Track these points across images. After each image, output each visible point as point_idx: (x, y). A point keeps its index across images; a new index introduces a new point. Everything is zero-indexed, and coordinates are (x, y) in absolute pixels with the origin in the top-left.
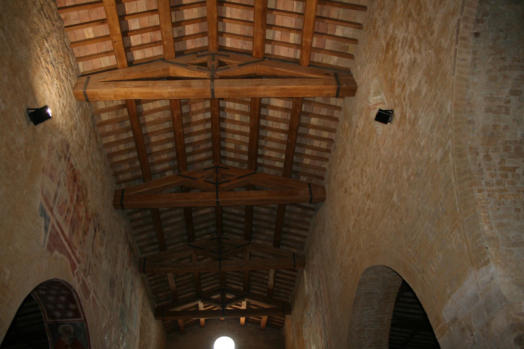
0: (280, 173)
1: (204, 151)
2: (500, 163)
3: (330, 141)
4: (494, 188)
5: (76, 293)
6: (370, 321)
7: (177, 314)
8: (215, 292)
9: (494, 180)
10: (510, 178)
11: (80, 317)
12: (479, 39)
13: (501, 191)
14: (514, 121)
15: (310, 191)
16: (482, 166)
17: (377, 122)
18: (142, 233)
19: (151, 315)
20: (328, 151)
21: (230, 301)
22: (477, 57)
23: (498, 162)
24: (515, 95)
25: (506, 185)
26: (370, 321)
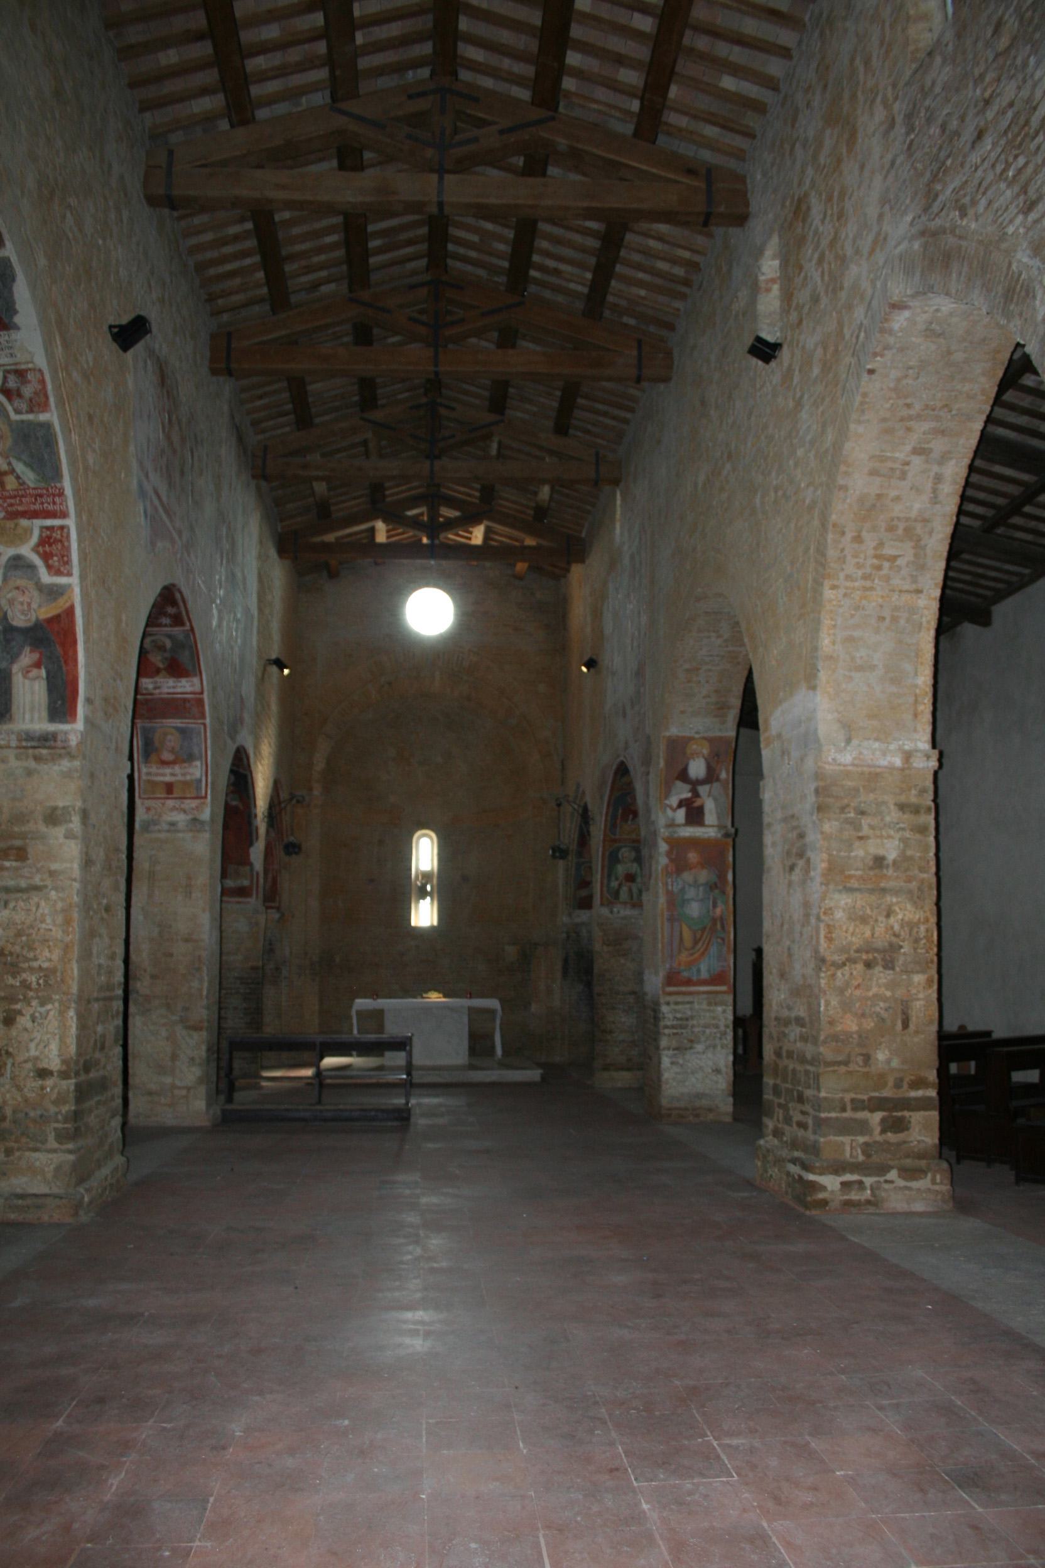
0: (579, 305)
1: (410, 243)
2: (875, 548)
3: (694, 266)
4: (857, 584)
5: (181, 593)
6: (711, 656)
7: (326, 547)
8: (415, 501)
9: (860, 573)
10: (885, 571)
11: (182, 624)
12: (873, 377)
13: (865, 589)
14: (911, 489)
15: (640, 358)
16: (846, 552)
17: (749, 357)
18: (260, 397)
19: (273, 553)
20: (687, 283)
21: (450, 524)
22: (867, 400)
23: (872, 546)
24: (920, 454)
25: (876, 581)
26: (711, 656)
